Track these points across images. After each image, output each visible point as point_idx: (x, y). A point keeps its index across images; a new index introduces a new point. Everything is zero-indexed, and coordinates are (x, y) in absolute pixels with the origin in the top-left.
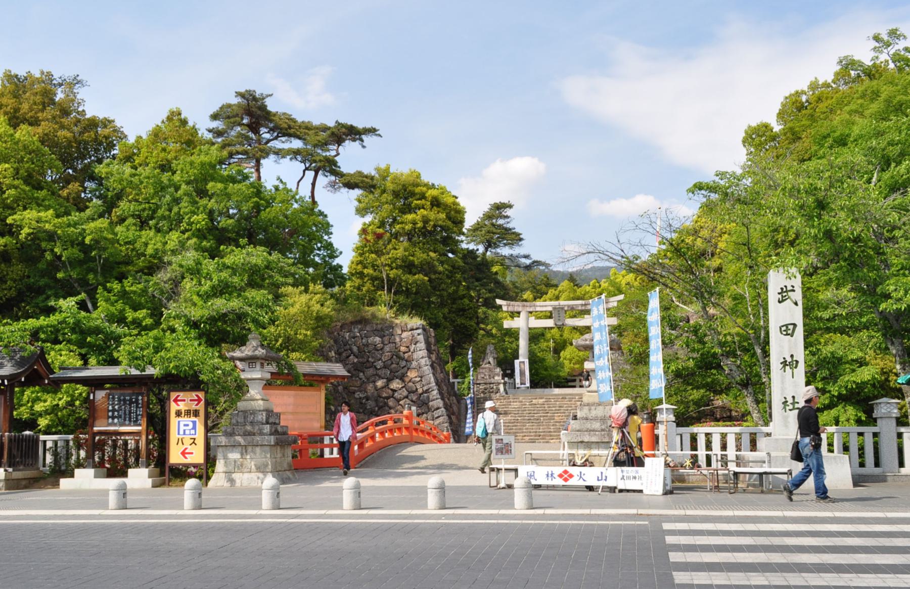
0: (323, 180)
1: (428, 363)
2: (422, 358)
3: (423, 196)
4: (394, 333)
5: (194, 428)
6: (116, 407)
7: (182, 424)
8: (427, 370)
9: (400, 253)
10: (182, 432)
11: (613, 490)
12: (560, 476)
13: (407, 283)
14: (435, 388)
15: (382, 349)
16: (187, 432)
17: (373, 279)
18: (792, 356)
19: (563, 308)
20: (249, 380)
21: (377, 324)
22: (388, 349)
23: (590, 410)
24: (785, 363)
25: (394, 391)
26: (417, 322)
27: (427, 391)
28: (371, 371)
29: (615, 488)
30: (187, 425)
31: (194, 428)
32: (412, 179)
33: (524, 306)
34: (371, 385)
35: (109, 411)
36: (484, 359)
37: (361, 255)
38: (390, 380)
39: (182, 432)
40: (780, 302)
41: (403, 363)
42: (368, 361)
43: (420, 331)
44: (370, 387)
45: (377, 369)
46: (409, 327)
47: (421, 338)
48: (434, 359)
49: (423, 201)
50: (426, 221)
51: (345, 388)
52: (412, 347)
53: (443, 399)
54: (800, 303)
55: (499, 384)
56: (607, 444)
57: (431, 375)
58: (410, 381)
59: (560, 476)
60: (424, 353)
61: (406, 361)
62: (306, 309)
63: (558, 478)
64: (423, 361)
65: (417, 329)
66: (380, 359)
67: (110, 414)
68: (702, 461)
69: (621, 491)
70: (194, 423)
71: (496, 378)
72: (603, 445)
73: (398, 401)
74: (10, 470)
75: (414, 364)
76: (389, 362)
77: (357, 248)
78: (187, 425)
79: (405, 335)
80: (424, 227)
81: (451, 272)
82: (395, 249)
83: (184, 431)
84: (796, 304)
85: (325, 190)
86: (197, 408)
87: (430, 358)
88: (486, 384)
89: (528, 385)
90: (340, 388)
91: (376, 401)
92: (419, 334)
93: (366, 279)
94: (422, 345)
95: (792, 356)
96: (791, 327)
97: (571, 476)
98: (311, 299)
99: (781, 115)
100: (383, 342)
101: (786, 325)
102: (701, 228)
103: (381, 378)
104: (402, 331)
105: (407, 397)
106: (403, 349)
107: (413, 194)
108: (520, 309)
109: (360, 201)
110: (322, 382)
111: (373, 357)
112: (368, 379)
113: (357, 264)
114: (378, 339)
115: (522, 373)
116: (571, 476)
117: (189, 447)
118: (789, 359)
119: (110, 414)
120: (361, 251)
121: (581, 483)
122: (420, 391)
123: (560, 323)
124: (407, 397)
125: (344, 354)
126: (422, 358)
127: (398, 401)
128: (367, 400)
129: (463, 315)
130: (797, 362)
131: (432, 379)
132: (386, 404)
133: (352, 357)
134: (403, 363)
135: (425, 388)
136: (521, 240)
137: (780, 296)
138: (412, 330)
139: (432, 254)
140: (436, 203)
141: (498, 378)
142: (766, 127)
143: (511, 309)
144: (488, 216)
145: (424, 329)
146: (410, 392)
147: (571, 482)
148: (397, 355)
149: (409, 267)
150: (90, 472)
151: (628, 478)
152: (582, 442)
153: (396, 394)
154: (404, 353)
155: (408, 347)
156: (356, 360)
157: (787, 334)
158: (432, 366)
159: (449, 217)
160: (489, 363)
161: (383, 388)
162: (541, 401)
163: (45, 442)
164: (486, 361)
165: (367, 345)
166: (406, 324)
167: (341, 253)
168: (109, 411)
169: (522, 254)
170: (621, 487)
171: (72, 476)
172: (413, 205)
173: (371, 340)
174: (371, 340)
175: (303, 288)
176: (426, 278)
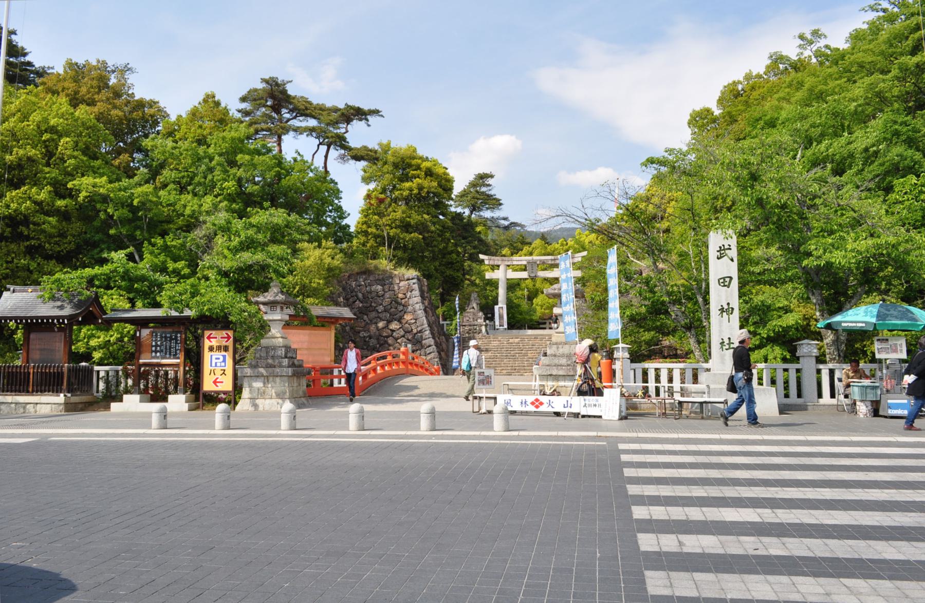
0: (334, 153)
1: (421, 308)
2: (417, 303)
3: (418, 167)
4: (393, 282)
5: (224, 361)
6: (159, 343)
7: (214, 358)
8: (421, 313)
9: (398, 215)
10: (213, 364)
11: (576, 415)
12: (532, 403)
13: (405, 240)
14: (428, 328)
15: (383, 295)
16: (218, 364)
17: (376, 237)
18: (728, 304)
19: (535, 263)
20: (270, 321)
21: (379, 275)
22: (388, 296)
23: (558, 348)
24: (722, 310)
25: (393, 331)
26: (412, 273)
27: (420, 332)
28: (373, 314)
29: (579, 414)
30: (219, 359)
31: (224, 361)
32: (409, 152)
33: (503, 260)
34: (374, 326)
35: (153, 346)
36: (469, 305)
37: (366, 216)
38: (389, 322)
39: (213, 364)
40: (718, 258)
41: (401, 308)
42: (371, 306)
43: (415, 281)
44: (373, 328)
45: (378, 312)
46: (406, 277)
47: (416, 286)
48: (426, 304)
49: (418, 172)
50: (421, 188)
51: (352, 328)
52: (409, 294)
53: (434, 338)
54: (735, 260)
55: (481, 325)
56: (571, 377)
57: (424, 318)
58: (406, 323)
59: (532, 403)
60: (418, 299)
61: (404, 306)
62: (319, 262)
63: (530, 405)
64: (417, 307)
65: (412, 279)
66: (381, 304)
67: (154, 349)
68: (652, 392)
69: (583, 416)
70: (224, 357)
71: (479, 321)
72: (568, 378)
73: (396, 339)
74: (69, 395)
75: (410, 308)
76: (389, 307)
77: (363, 211)
78: (219, 359)
79: (402, 284)
80: (419, 193)
81: (441, 231)
82: (395, 211)
83: (216, 363)
84: (732, 260)
85: (336, 162)
86: (227, 344)
87: (423, 303)
88: (470, 325)
89: (506, 326)
90: (348, 328)
91: (378, 339)
92: (414, 284)
93: (370, 237)
94: (417, 293)
95: (728, 304)
96: (728, 280)
97: (541, 404)
98: (323, 253)
99: (721, 101)
100: (383, 290)
101: (724, 278)
102: (653, 195)
103: (382, 320)
104: (400, 281)
105: (403, 336)
106: (400, 296)
107: (410, 166)
108: (499, 263)
109: (365, 171)
110: (333, 323)
111: (375, 303)
112: (371, 321)
113: (363, 224)
114: (379, 287)
115: (501, 317)
116: (541, 404)
117: (220, 377)
118: (726, 307)
119: (154, 349)
120: (366, 213)
121: (550, 410)
122: (415, 331)
123: (533, 275)
124: (403, 336)
125: (351, 300)
126: (417, 303)
127: (396, 339)
128: (370, 338)
129: (451, 267)
130: (733, 309)
131: (425, 322)
132: (386, 342)
133: (357, 302)
134: (401, 308)
135: (419, 329)
136: (501, 204)
137: (719, 254)
138: (408, 279)
139: (426, 216)
140: (429, 173)
141: (481, 321)
142: (708, 111)
143: (492, 263)
144: (473, 185)
145: (419, 279)
146: (406, 332)
147: (541, 409)
148: (395, 301)
149: (406, 227)
150: (136, 397)
151: (590, 405)
152: (551, 375)
153: (394, 334)
154: (402, 299)
155: (405, 294)
156: (361, 305)
157: (725, 286)
158: (425, 310)
159: (440, 185)
160: (473, 308)
161: (383, 328)
162: (517, 340)
163: (98, 372)
164: (470, 307)
165: (371, 292)
166: (403, 275)
167: (349, 214)
168: (153, 346)
169: (501, 216)
170: (582, 413)
171: (121, 400)
172: (410, 175)
173: (373, 288)
174: (373, 288)
175: (317, 244)
176: (421, 236)
